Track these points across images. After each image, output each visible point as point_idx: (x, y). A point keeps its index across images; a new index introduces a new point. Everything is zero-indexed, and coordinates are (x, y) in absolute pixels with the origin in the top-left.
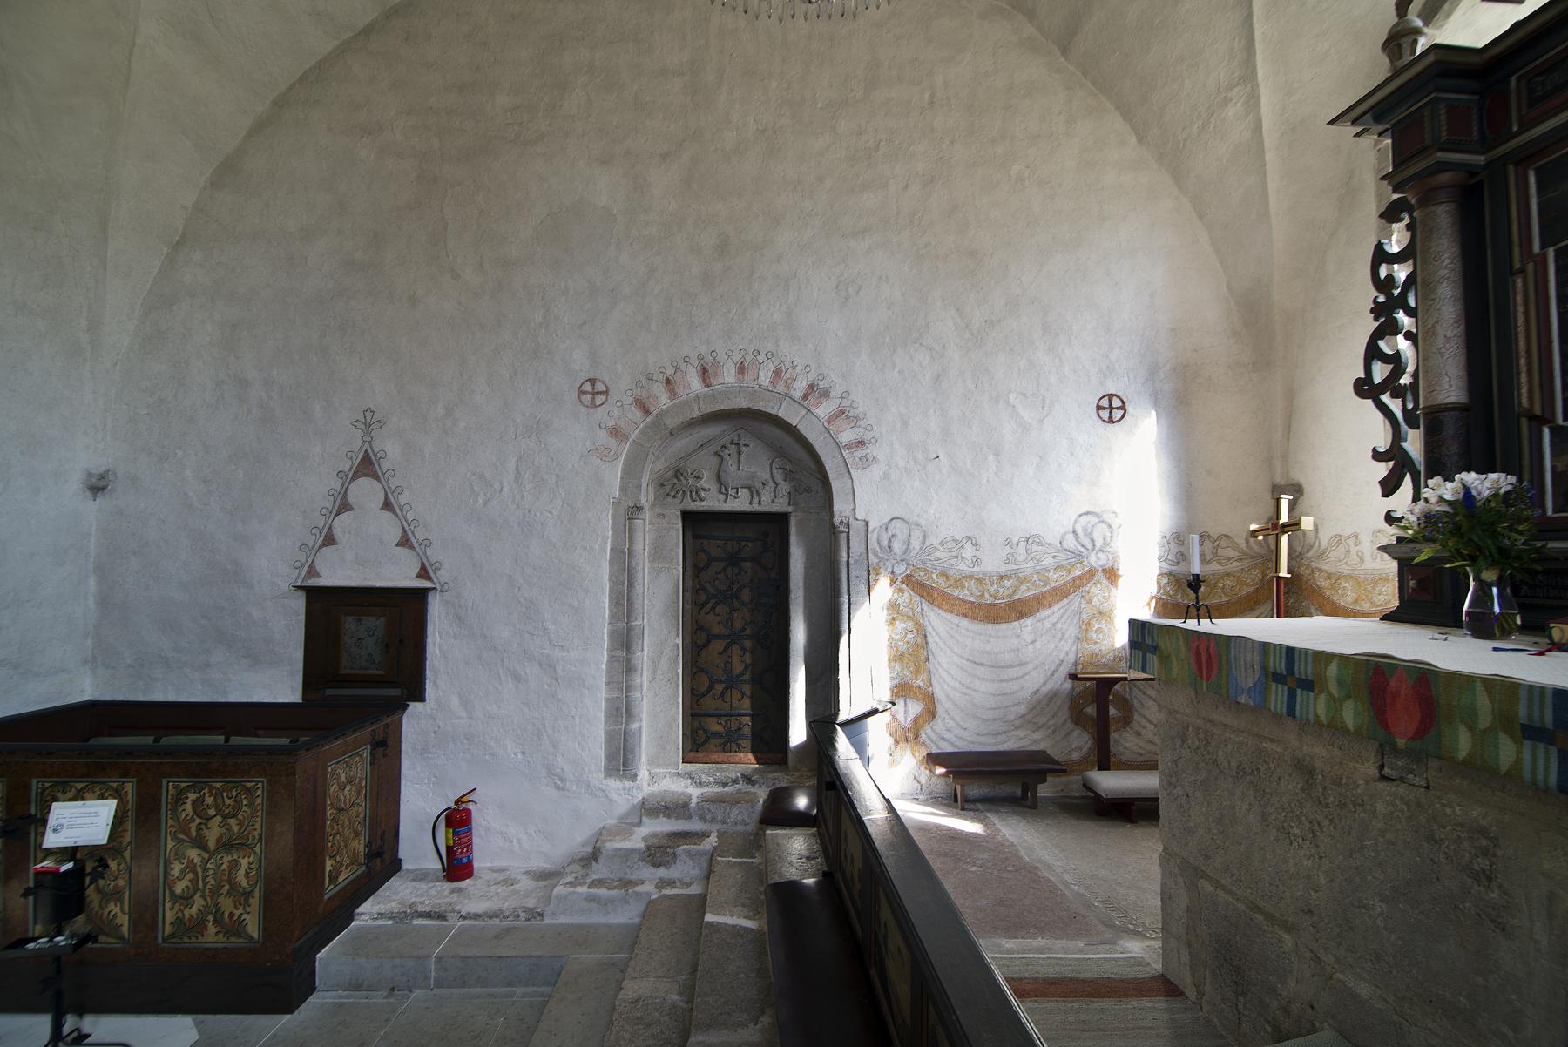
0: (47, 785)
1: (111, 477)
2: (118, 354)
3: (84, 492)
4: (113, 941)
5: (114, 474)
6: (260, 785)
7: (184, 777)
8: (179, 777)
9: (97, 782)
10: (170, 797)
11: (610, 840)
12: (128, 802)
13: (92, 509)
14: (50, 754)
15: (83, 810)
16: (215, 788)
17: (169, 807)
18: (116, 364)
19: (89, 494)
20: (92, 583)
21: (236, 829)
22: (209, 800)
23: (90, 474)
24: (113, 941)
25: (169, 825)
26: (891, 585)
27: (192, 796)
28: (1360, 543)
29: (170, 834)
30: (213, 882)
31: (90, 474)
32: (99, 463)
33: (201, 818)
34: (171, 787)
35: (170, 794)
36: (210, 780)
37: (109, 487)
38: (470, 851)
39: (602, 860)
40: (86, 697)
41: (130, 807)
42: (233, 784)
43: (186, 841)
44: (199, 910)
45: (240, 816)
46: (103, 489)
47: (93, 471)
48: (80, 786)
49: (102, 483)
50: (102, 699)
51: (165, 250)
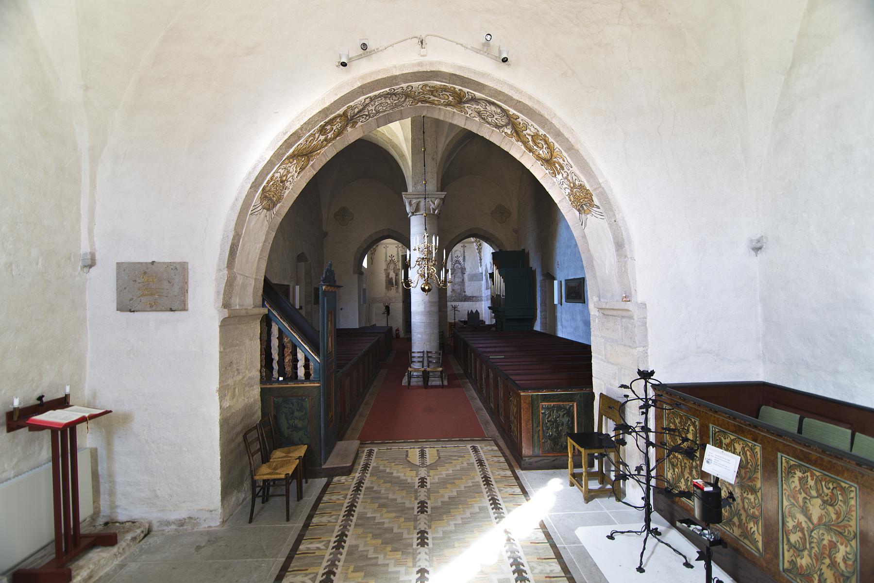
0: (717, 430)
1: (765, 240)
2: (761, 161)
3: (749, 251)
4: (753, 548)
5: (766, 238)
6: (853, 489)
7: (793, 457)
8: (788, 455)
9: (742, 439)
10: (783, 468)
11: (146, 498)
12: (758, 459)
13: (755, 262)
14: (716, 412)
15: (721, 455)
16: (816, 475)
17: (784, 475)
18: (761, 167)
19: (753, 253)
20: (759, 308)
21: (834, 517)
22: (811, 483)
23: (752, 241)
24: (753, 548)
25: (784, 488)
26: (504, 517)
27: (799, 474)
28: (258, 161)
29: (785, 495)
30: (816, 549)
31: (752, 241)
32: (756, 234)
33: (806, 494)
34: (784, 461)
35: (783, 465)
36: (813, 468)
37: (764, 247)
38: (91, 461)
39: (209, 525)
40: (761, 379)
41: (759, 463)
42: (831, 479)
43: (796, 507)
44: (807, 565)
45: (836, 507)
46: (760, 248)
47: (753, 238)
48: (732, 437)
49: (759, 245)
50: (770, 382)
51: (783, 78)
